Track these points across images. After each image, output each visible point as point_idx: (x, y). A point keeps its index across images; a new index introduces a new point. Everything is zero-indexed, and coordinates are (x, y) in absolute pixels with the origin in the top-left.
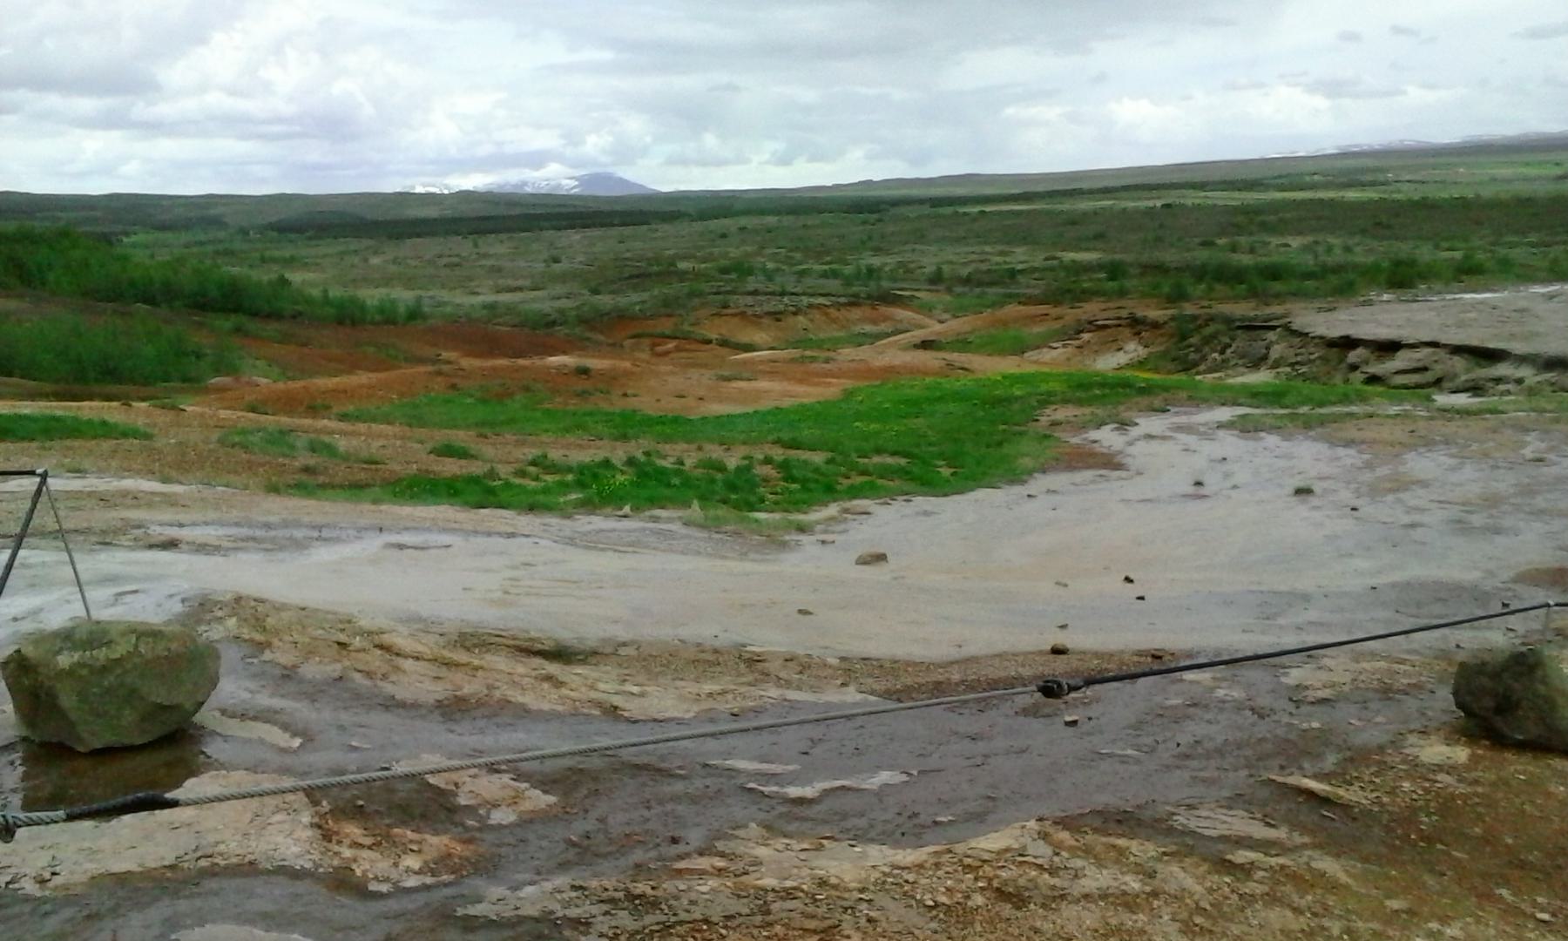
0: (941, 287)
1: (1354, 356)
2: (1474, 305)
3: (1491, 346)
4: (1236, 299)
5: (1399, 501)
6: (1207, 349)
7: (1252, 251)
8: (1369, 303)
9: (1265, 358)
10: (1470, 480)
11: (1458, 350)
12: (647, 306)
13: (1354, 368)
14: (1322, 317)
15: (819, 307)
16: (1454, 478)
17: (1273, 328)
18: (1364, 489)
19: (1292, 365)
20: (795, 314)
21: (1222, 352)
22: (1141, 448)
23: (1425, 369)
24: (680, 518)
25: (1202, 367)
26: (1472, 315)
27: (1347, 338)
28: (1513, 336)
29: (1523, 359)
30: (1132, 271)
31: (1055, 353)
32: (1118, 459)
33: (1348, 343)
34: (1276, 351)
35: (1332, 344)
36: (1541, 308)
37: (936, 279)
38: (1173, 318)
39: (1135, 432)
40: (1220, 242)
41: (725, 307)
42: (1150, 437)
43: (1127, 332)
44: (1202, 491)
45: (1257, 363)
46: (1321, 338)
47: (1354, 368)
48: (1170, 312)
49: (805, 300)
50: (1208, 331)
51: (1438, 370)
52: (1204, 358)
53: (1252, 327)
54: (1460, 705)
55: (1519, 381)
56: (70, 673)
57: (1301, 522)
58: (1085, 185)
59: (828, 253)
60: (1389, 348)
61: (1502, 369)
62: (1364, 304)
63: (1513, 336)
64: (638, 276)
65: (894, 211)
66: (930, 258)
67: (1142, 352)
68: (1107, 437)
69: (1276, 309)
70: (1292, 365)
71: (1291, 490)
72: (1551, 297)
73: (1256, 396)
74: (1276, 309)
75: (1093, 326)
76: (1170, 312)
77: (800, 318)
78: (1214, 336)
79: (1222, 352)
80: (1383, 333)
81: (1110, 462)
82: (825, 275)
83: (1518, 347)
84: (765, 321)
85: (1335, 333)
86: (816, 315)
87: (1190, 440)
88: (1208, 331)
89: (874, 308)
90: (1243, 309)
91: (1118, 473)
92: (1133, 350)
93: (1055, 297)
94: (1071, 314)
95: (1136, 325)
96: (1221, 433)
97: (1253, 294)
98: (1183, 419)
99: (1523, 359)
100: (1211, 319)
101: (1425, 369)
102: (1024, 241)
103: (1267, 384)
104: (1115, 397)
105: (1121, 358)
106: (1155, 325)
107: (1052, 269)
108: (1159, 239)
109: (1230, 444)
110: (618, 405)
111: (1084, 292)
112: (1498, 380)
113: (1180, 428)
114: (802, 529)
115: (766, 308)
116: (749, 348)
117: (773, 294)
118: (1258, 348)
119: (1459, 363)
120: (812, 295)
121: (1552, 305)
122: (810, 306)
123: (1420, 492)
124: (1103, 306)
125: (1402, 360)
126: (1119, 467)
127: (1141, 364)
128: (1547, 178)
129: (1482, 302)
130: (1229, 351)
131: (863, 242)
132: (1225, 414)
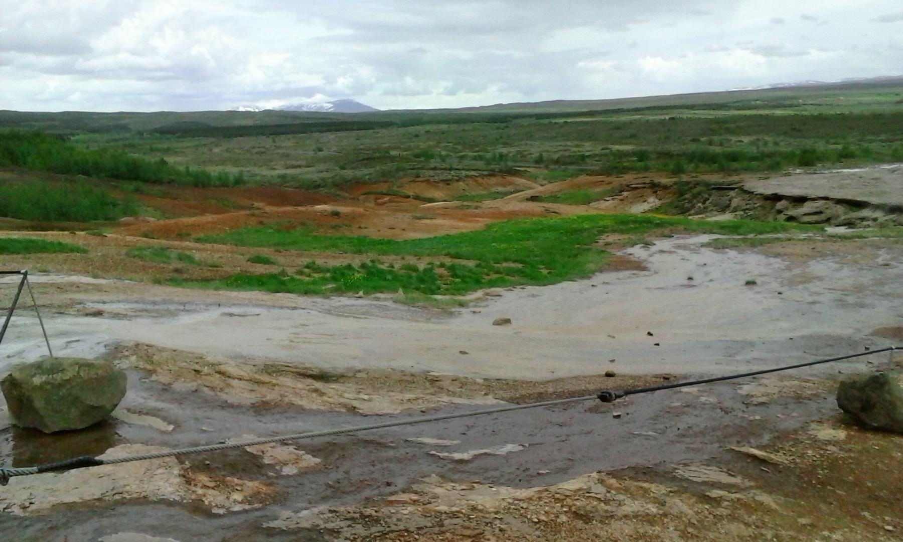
0: (542, 165)
1: (780, 205)
2: (849, 176)
3: (859, 199)
4: (712, 172)
5: (806, 288)
6: (695, 201)
7: (721, 144)
8: (789, 175)
9: (728, 206)
10: (847, 276)
11: (839, 202)
12: (373, 176)
13: (780, 212)
14: (761, 183)
15: (471, 177)
16: (837, 275)
17: (733, 189)
18: (785, 282)
19: (744, 210)
20: (458, 181)
21: (704, 203)
22: (657, 258)
23: (821, 213)
24: (392, 298)
25: (692, 212)
26: (848, 181)
27: (776, 194)
28: (871, 194)
29: (877, 207)
30: (652, 156)
31: (607, 203)
32: (644, 264)
33: (776, 198)
34: (735, 202)
35: (767, 198)
36: (887, 177)
37: (539, 161)
38: (675, 183)
39: (653, 249)
40: (703, 139)
41: (418, 177)
42: (662, 252)
43: (649, 191)
44: (692, 283)
45: (724, 209)
46: (761, 194)
47: (780, 212)
48: (674, 180)
49: (464, 173)
50: (696, 190)
51: (828, 213)
52: (693, 206)
53: (721, 189)
54: (841, 406)
55: (875, 220)
56: (41, 387)
57: (749, 300)
58: (625, 107)
59: (477, 146)
60: (800, 200)
61: (865, 213)
62: (786, 175)
63: (871, 194)
64: (367, 159)
65: (515, 121)
66: (535, 149)
67: (658, 203)
68: (638, 252)
69: (735, 178)
70: (744, 210)
71: (743, 282)
72: (893, 171)
73: (723, 228)
74: (735, 178)
75: (629, 188)
76: (674, 180)
77: (461, 183)
78: (699, 194)
79: (704, 203)
80: (797, 192)
81: (639, 266)
82: (475, 158)
83: (874, 200)
84: (441, 185)
85: (769, 192)
86: (470, 181)
87: (686, 253)
88: (696, 190)
89: (503, 178)
90: (716, 178)
91: (644, 272)
92: (653, 201)
93: (607, 171)
94: (617, 181)
95: (654, 187)
96: (703, 249)
97: (722, 169)
98: (681, 242)
99: (877, 207)
100: (697, 184)
101: (821, 213)
102: (590, 139)
103: (730, 221)
104: (642, 229)
105: (646, 206)
106: (665, 187)
107: (606, 155)
108: (667, 138)
109: (708, 255)
110: (356, 233)
111: (624, 168)
112: (863, 219)
113: (679, 247)
114: (462, 305)
115: (441, 177)
116: (431, 200)
117: (445, 169)
118: (725, 200)
119: (840, 209)
120: (468, 170)
121: (894, 176)
122: (467, 176)
123: (818, 283)
124: (635, 176)
125: (807, 207)
126: (644, 269)
127: (657, 210)
128: (891, 103)
129: (853, 174)
130: (708, 202)
131: (497, 140)
132: (705, 238)
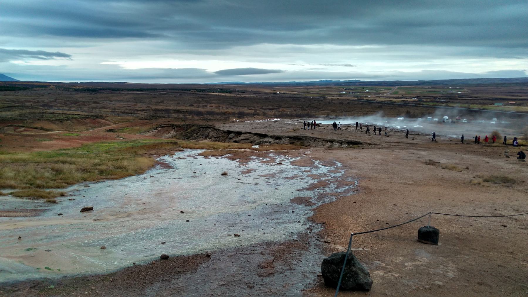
2: (258, 123)
5: (250, 176)
8: (234, 122)
10: (267, 169)
12: (13, 116)
13: (230, 139)
14: (222, 126)
15: (75, 118)
16: (261, 169)
17: (210, 128)
18: (240, 173)
19: (215, 138)
20: (67, 120)
21: (197, 134)
22: (177, 161)
23: (248, 139)
24: (11, 194)
29: (271, 137)
30: (171, 112)
31: (150, 133)
32: (171, 165)
33: (229, 132)
35: (225, 132)
36: (273, 124)
39: (175, 157)
40: (195, 105)
41: (42, 117)
42: (180, 158)
44: (196, 174)
45: (206, 137)
47: (230, 139)
48: (182, 123)
50: (193, 128)
51: (251, 139)
52: (192, 136)
53: (205, 128)
54: (322, 273)
55: (270, 142)
57: (224, 185)
58: (158, 88)
59: (79, 102)
61: (266, 139)
62: (232, 122)
64: (10, 107)
67: (175, 133)
68: (167, 159)
69: (211, 123)
70: (215, 138)
72: (276, 122)
73: (209, 147)
74: (211, 123)
76: (182, 123)
78: (194, 130)
79: (197, 134)
80: (238, 130)
81: (167, 166)
83: (270, 134)
85: (226, 130)
87: (191, 159)
88: (193, 128)
91: (171, 170)
92: (173, 133)
94: (155, 123)
98: (188, 153)
99: (271, 137)
101: (248, 139)
102: (141, 102)
104: (173, 147)
107: (149, 110)
108: (178, 104)
109: (201, 159)
111: (158, 117)
112: (266, 142)
113: (188, 156)
114: (62, 195)
115: (58, 118)
116: (51, 130)
118: (206, 133)
119: (256, 137)
121: (276, 124)
122: (73, 118)
123: (254, 173)
125: (242, 137)
126: (171, 167)
128: (271, 93)
129: (260, 123)
132: (200, 151)
